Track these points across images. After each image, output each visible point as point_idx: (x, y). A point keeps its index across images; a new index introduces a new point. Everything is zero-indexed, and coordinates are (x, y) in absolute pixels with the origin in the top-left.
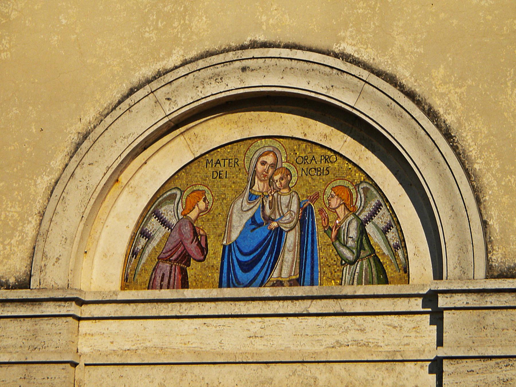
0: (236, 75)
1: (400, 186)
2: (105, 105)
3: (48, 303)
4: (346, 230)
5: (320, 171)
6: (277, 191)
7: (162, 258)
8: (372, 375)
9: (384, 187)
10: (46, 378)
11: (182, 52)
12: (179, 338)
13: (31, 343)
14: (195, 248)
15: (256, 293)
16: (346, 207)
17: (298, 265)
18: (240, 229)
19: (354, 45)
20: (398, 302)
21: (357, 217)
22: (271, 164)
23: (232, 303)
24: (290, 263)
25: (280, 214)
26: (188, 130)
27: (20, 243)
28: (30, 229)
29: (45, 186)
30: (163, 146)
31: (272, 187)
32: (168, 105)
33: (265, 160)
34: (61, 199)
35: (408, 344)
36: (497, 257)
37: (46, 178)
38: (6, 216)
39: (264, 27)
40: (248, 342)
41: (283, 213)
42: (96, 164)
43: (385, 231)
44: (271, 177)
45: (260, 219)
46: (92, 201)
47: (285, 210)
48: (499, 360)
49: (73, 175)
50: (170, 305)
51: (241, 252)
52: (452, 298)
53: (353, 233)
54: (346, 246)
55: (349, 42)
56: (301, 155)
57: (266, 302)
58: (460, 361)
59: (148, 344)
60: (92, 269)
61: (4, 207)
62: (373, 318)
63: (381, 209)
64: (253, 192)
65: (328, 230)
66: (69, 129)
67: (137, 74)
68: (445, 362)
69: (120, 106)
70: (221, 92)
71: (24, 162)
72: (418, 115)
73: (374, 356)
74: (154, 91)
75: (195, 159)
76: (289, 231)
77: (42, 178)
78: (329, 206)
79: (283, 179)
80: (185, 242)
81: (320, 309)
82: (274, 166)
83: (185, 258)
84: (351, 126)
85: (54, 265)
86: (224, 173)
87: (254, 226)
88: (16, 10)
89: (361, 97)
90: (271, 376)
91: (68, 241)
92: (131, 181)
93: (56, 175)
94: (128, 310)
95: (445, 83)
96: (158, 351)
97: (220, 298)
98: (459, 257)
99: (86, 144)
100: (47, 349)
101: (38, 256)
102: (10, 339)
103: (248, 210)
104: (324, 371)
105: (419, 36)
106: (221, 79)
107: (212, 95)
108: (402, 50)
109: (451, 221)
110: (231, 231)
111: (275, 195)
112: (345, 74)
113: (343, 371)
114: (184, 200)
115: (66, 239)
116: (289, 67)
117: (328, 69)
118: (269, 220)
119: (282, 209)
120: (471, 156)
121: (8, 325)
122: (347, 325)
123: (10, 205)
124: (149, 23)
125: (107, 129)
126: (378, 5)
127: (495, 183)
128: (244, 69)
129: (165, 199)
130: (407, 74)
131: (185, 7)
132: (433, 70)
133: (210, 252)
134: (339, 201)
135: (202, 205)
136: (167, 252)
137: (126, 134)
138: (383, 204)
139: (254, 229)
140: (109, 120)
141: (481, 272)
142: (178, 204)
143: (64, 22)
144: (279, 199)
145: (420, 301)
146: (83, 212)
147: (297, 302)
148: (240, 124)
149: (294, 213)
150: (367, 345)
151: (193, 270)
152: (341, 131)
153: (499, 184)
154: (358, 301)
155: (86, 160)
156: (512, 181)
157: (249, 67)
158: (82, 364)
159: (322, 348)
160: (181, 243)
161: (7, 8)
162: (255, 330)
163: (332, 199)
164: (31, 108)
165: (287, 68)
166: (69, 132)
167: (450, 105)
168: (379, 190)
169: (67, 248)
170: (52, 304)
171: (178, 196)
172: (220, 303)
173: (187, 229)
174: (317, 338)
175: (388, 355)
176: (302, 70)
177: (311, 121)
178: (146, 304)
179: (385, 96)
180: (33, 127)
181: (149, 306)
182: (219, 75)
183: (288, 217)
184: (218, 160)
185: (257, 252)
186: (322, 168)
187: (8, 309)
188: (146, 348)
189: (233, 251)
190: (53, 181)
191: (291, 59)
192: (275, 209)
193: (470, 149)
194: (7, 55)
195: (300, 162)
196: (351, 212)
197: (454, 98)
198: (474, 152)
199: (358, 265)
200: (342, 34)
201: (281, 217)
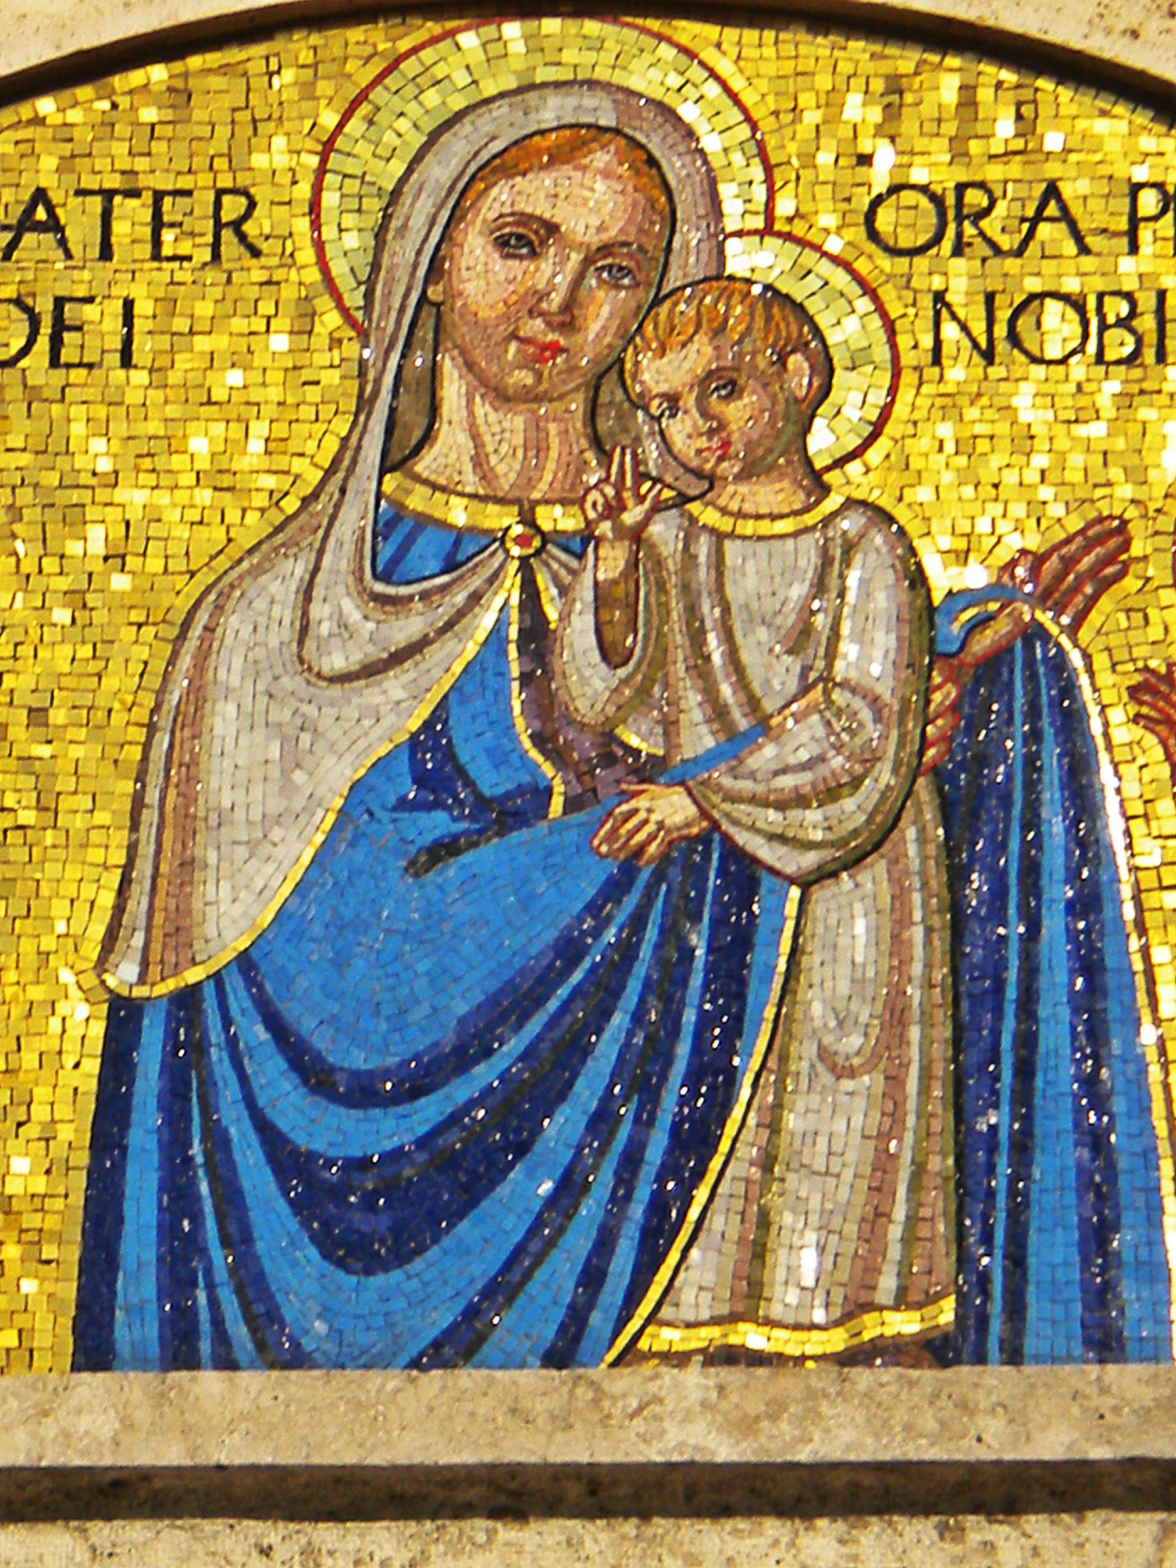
6: (683, 499)
15: (563, 1421)
17: (937, 1202)
18: (298, 851)
22: (605, 249)
23: (272, 1532)
24: (848, 1190)
25: (718, 713)
31: (620, 460)
33: (542, 209)
41: (753, 704)
44: (613, 368)
45: (508, 749)
47: (775, 676)
56: (918, 176)
57: (660, 1525)
64: (418, 500)
72: (104, 1425)
76: (826, 874)
79: (733, 390)
82: (634, 263)
86: (103, 320)
87: (439, 823)
97: (146, 1475)
103: (371, 671)
110: (188, 865)
111: (664, 532)
118: (607, 771)
119: (732, 655)
139: (443, 850)
144: (703, 575)
147: (999, 1532)
149: (875, 702)
172: (136, 1531)
183: (803, 738)
184: (40, 195)
185: (485, 1074)
189: (217, 1054)
192: (659, 661)
195: (906, 240)
201: (733, 746)
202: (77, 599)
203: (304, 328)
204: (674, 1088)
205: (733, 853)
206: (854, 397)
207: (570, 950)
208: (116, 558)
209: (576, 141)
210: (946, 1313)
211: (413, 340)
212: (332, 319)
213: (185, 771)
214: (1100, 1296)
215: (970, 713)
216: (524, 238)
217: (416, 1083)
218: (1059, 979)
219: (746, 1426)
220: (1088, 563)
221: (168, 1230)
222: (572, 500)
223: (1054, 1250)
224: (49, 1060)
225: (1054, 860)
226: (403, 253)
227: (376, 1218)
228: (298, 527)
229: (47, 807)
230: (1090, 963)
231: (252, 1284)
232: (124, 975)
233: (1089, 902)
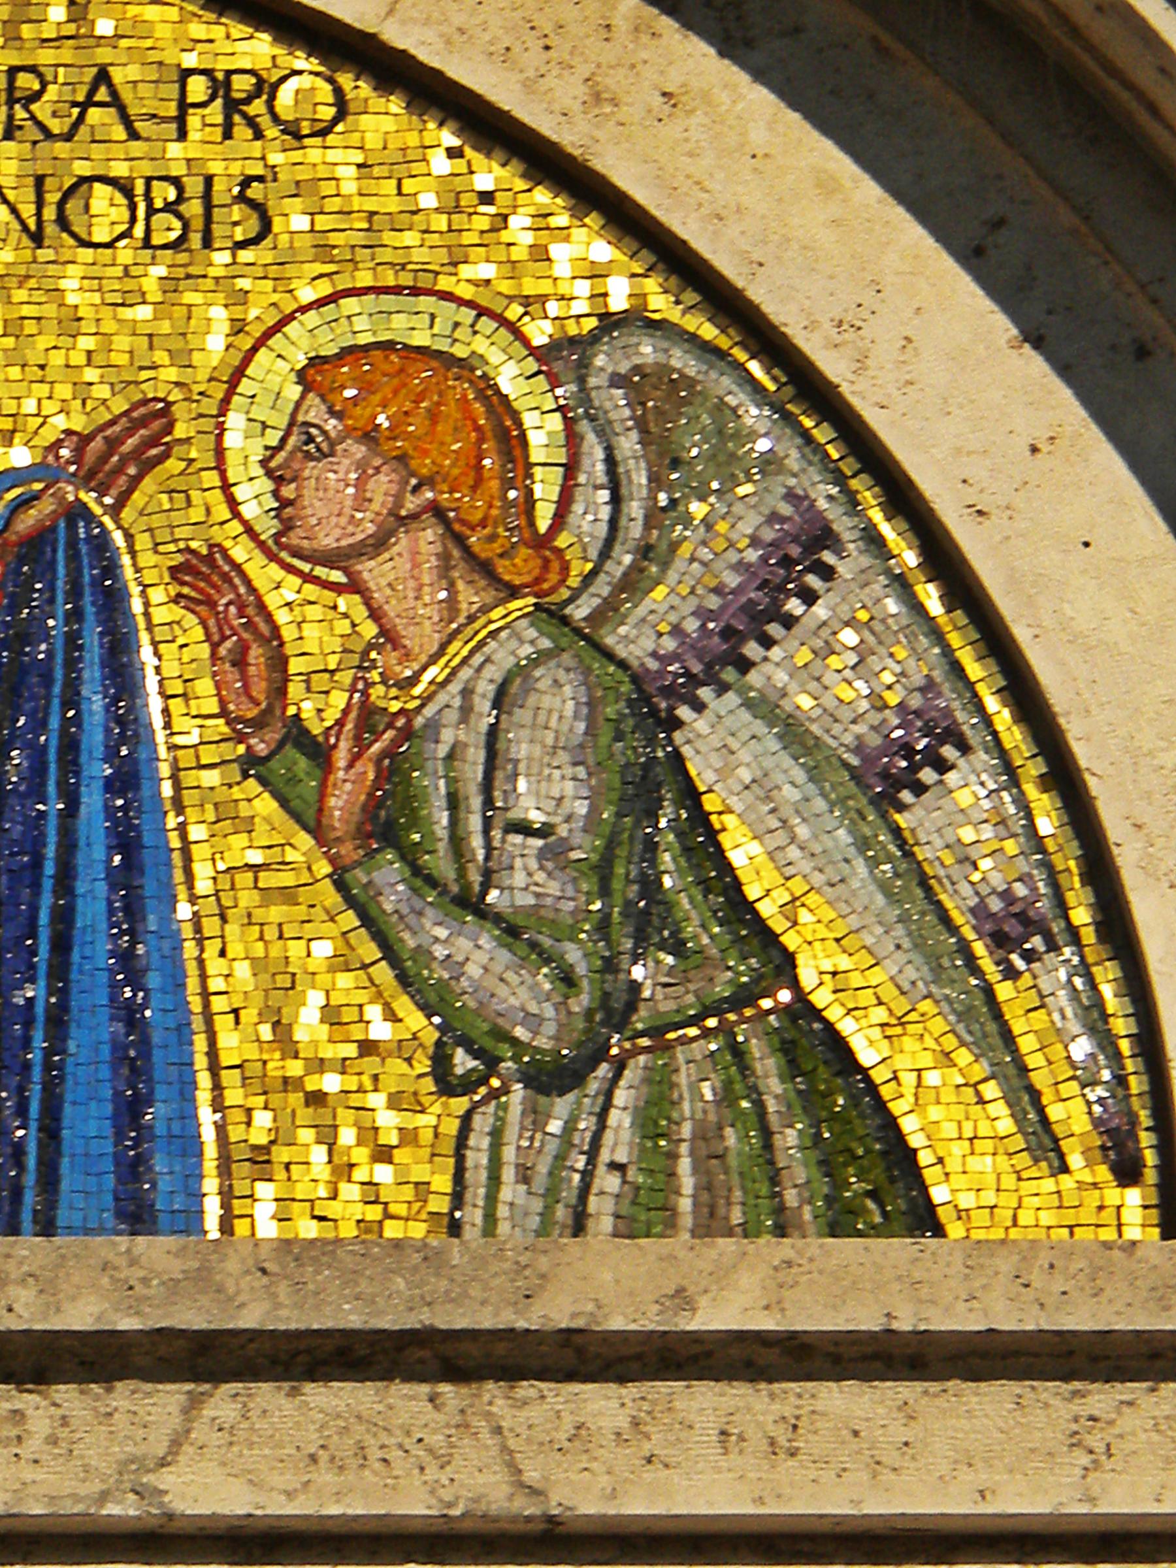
1: (1034, 366)
4: (476, 756)
5: (169, 208)
9: (861, 363)
10: (1044, 447)
16: (460, 540)
20: (1128, 1421)
43: (890, 776)
53: (550, 790)
54: (481, 912)
63: (827, 573)
65: (277, 751)
78: (287, 526)
81: (290, 1480)
134: (382, 486)
138: (843, 525)
154: (703, 1401)
163: (311, 469)
168: (808, 389)
186: (194, 186)
196: (514, 592)
199: (621, 1097)
214: (133, 1169)
218: (96, 854)
220: (129, 447)
225: (94, 738)
233: (128, 779)
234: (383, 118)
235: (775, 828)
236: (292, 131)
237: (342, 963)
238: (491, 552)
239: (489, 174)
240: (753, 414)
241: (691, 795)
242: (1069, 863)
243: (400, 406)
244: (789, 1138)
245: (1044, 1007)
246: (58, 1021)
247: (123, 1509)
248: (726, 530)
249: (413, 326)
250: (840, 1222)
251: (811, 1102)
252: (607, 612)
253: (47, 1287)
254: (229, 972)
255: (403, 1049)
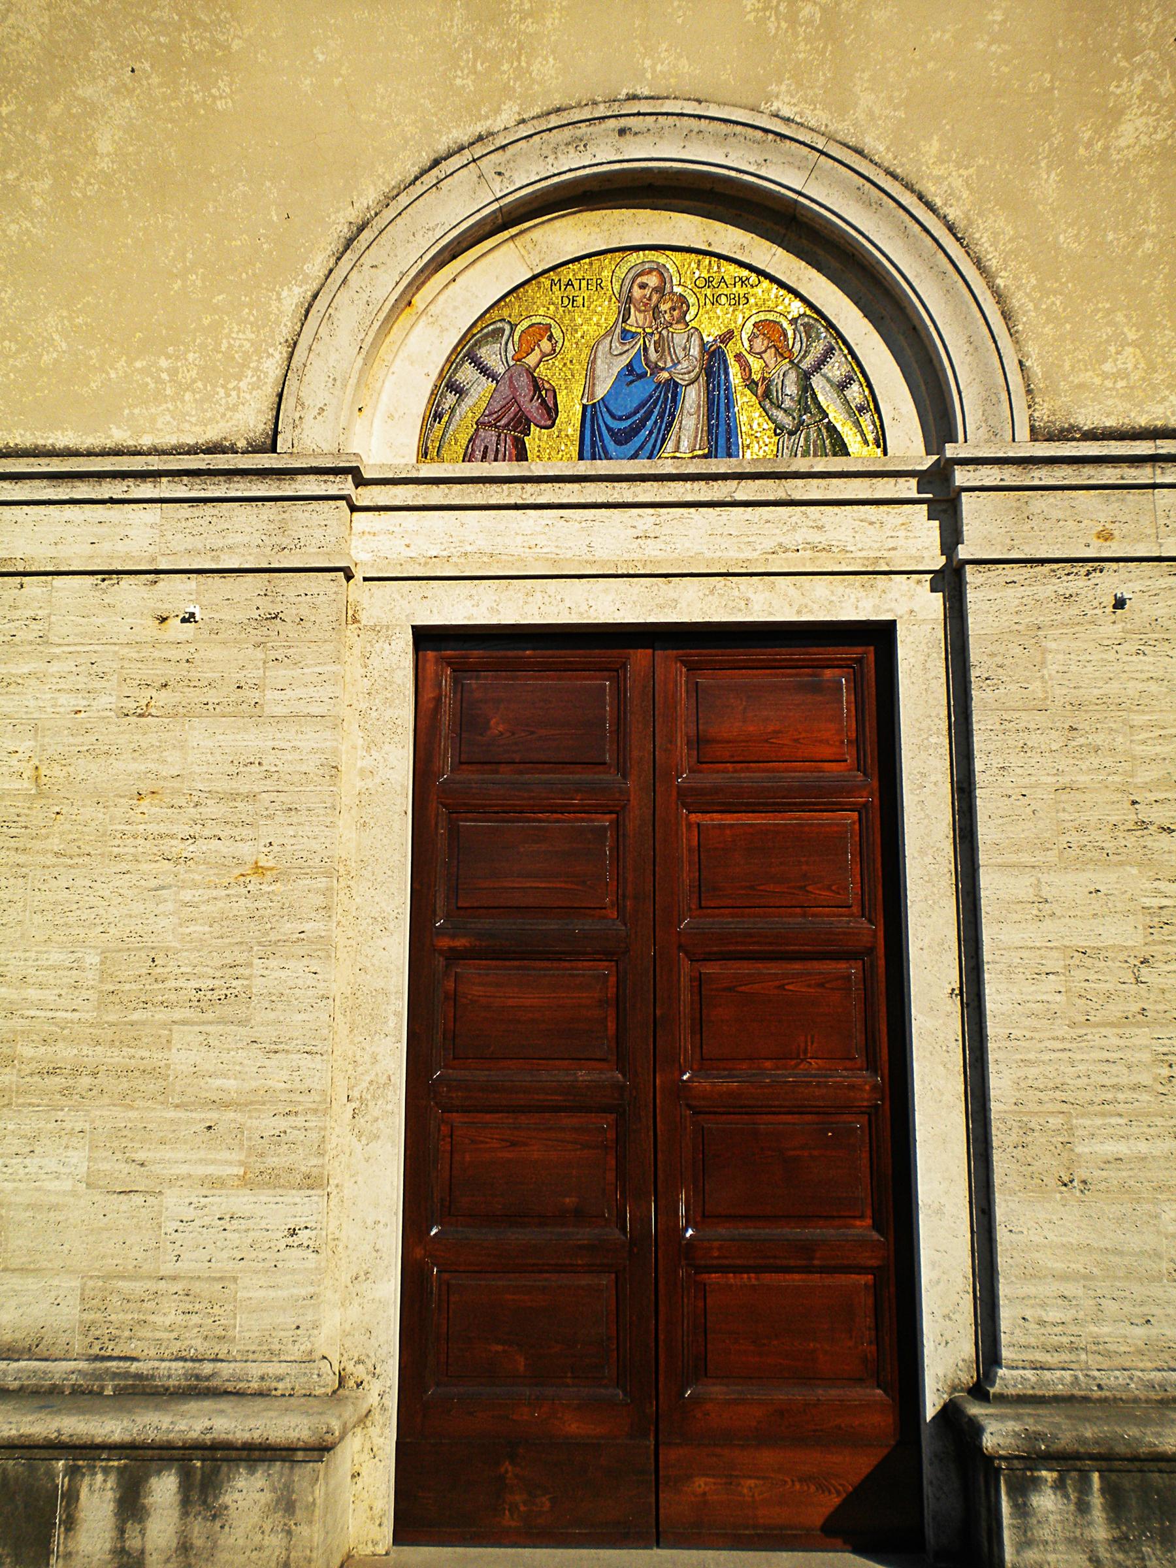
0: (609, 140)
2: (393, 183)
3: (306, 477)
7: (483, 424)
8: (840, 594)
11: (516, 109)
12: (519, 539)
13: (274, 540)
14: (538, 409)
19: (795, 105)
21: (797, 366)
23: (608, 484)
24: (692, 432)
25: (672, 360)
26: (522, 232)
27: (255, 387)
28: (272, 367)
29: (295, 302)
30: (483, 255)
32: (498, 183)
34: (327, 317)
35: (894, 549)
36: (1043, 413)
37: (296, 290)
38: (230, 347)
39: (649, 76)
40: (635, 546)
42: (383, 268)
43: (842, 386)
44: (657, 306)
46: (376, 325)
47: (681, 354)
48: (1055, 566)
49: (344, 281)
50: (505, 486)
51: (613, 416)
52: (977, 473)
53: (792, 389)
55: (787, 99)
58: (993, 567)
59: (469, 549)
60: (371, 435)
61: (226, 331)
62: (836, 509)
64: (627, 328)
65: (751, 384)
66: (333, 217)
67: (444, 138)
68: (968, 567)
69: (423, 179)
70: (584, 167)
71: (258, 265)
73: (843, 564)
74: (479, 158)
75: (535, 277)
77: (290, 289)
80: (521, 400)
82: (660, 290)
83: (522, 424)
84: (783, 231)
85: (315, 418)
86: (580, 299)
87: (631, 378)
88: (240, 38)
89: (813, 175)
90: (675, 596)
91: (338, 383)
92: (431, 307)
93: (315, 286)
94: (436, 495)
95: (943, 162)
96: (485, 559)
98: (984, 411)
99: (367, 235)
100: (303, 549)
101: (288, 404)
102: (239, 534)
103: (621, 354)
104: (761, 588)
105: (897, 94)
106: (585, 146)
107: (571, 170)
108: (870, 113)
109: (968, 359)
112: (788, 142)
113: (792, 587)
114: (516, 338)
115: (335, 380)
116: (696, 130)
117: (759, 134)
118: (656, 369)
120: (990, 266)
121: (236, 513)
122: (794, 519)
123: (236, 329)
124: (462, 64)
125: (400, 214)
126: (830, 48)
127: (1031, 306)
128: (622, 132)
129: (487, 335)
130: (882, 148)
131: (519, 42)
132: (922, 143)
133: (562, 417)
134: (766, 342)
135: (546, 345)
136: (490, 415)
137: (431, 225)
139: (632, 382)
140: (404, 200)
141: (1023, 433)
142: (506, 344)
143: (321, 58)
145: (913, 482)
146: (362, 340)
148: (605, 227)
150: (828, 549)
151: (535, 439)
152: (767, 239)
153: (1036, 308)
155: (367, 260)
156: (1058, 303)
157: (630, 129)
158: (359, 575)
159: (755, 555)
160: (514, 399)
161: (224, 34)
162: (646, 527)
164: (268, 184)
165: (691, 131)
166: (334, 223)
167: (951, 193)
168: (830, 325)
169: (336, 393)
170: (312, 477)
171: (507, 333)
173: (524, 380)
174: (747, 540)
175: (866, 563)
176: (716, 135)
177: (718, 225)
178: (465, 486)
179: (852, 174)
180: (273, 213)
181: (470, 488)
182: (581, 140)
183: (685, 364)
185: (639, 415)
187: (237, 486)
188: (466, 554)
190: (309, 293)
191: (700, 117)
192: (663, 351)
193: (989, 257)
194: (226, 103)
197: (958, 183)
198: (994, 261)
200: (773, 88)
201: (675, 365)
202: (577, 343)
203: (610, 301)
204: (666, 418)
205: (675, 382)
206: (693, 311)
207: (651, 396)
208: (582, 337)
209: (651, 271)
210: (706, 451)
211: (627, 302)
212: (614, 299)
213: (593, 370)
214: (729, 448)
215: (710, 360)
216: (643, 286)
217: (628, 418)
218: (723, 401)
219: (677, 468)
220: (727, 337)
221: (592, 439)
222: (651, 327)
223: (722, 441)
224: (574, 414)
225: (722, 382)
226: (624, 289)
227: (622, 438)
228: (609, 332)
229: (573, 376)
230: (727, 397)
231: (604, 447)
232: (585, 401)
233: (727, 389)
234: (766, 283)
235: (825, 394)
236: (752, 286)
237: (760, 416)
238: (782, 352)
239: (782, 292)
240: (822, 329)
241: (813, 389)
242: (870, 399)
243: (768, 329)
244: (827, 442)
245: (866, 421)
246: (717, 426)
247: (729, 499)
248: (818, 348)
249: (770, 317)
250: (835, 455)
251: (830, 436)
252: (800, 361)
253: (717, 466)
254: (743, 419)
255: (770, 429)
